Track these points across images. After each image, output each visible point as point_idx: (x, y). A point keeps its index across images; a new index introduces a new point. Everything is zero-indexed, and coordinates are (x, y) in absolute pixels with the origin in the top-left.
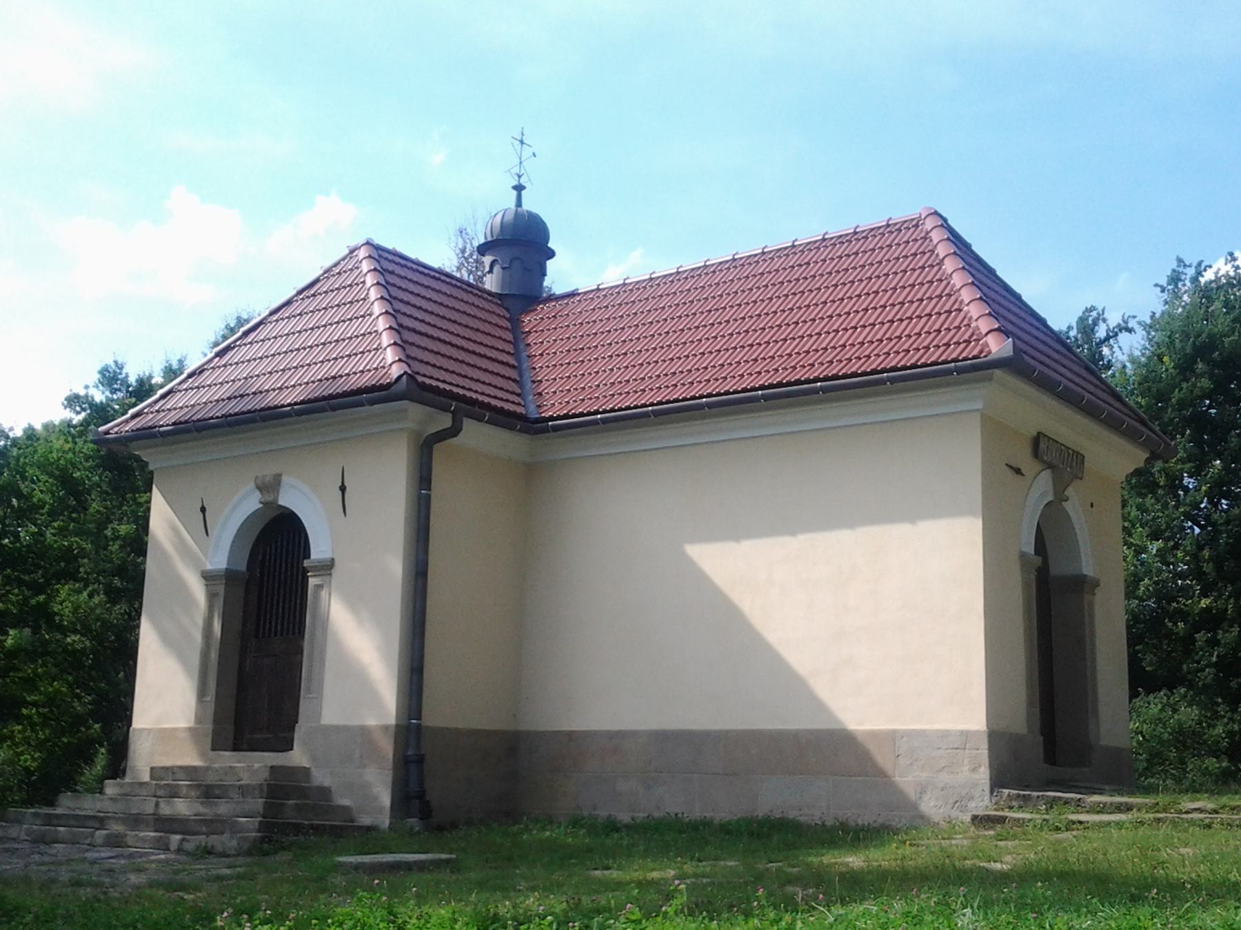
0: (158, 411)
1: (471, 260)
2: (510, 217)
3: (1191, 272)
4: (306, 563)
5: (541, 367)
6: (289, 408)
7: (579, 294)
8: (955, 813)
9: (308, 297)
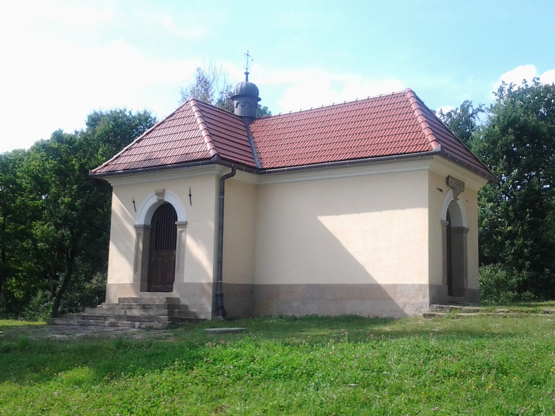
0: (115, 164)
1: (202, 82)
2: (244, 85)
3: (507, 87)
4: (176, 223)
5: (260, 147)
6: (170, 165)
7: (272, 117)
8: (417, 313)
9: (171, 120)
